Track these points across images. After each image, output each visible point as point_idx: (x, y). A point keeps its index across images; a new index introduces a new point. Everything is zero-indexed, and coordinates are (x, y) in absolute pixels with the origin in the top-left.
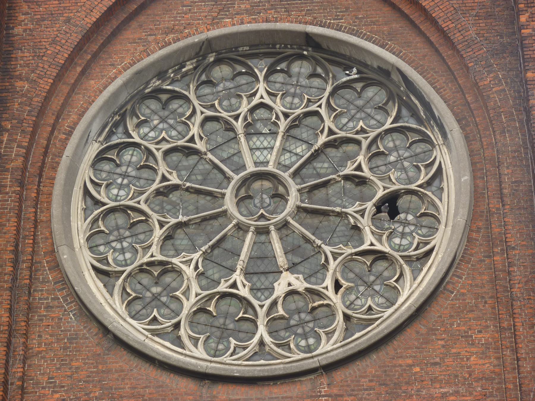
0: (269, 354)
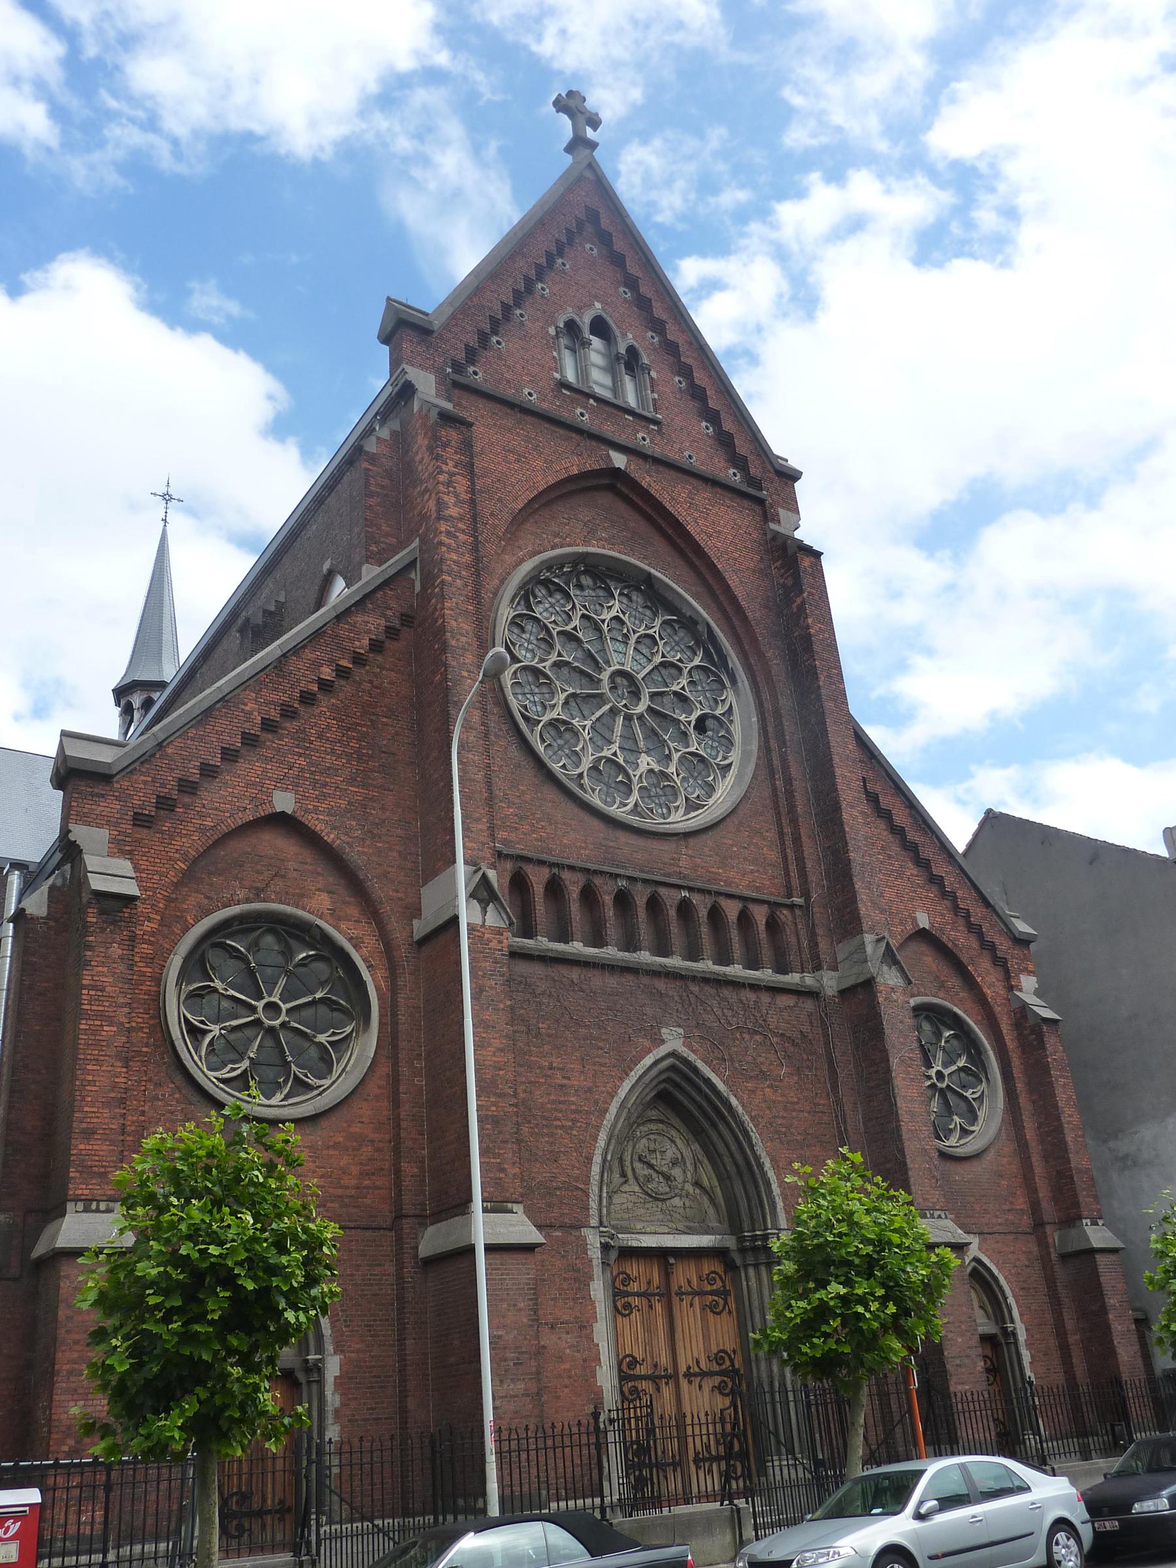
0: (639, 813)
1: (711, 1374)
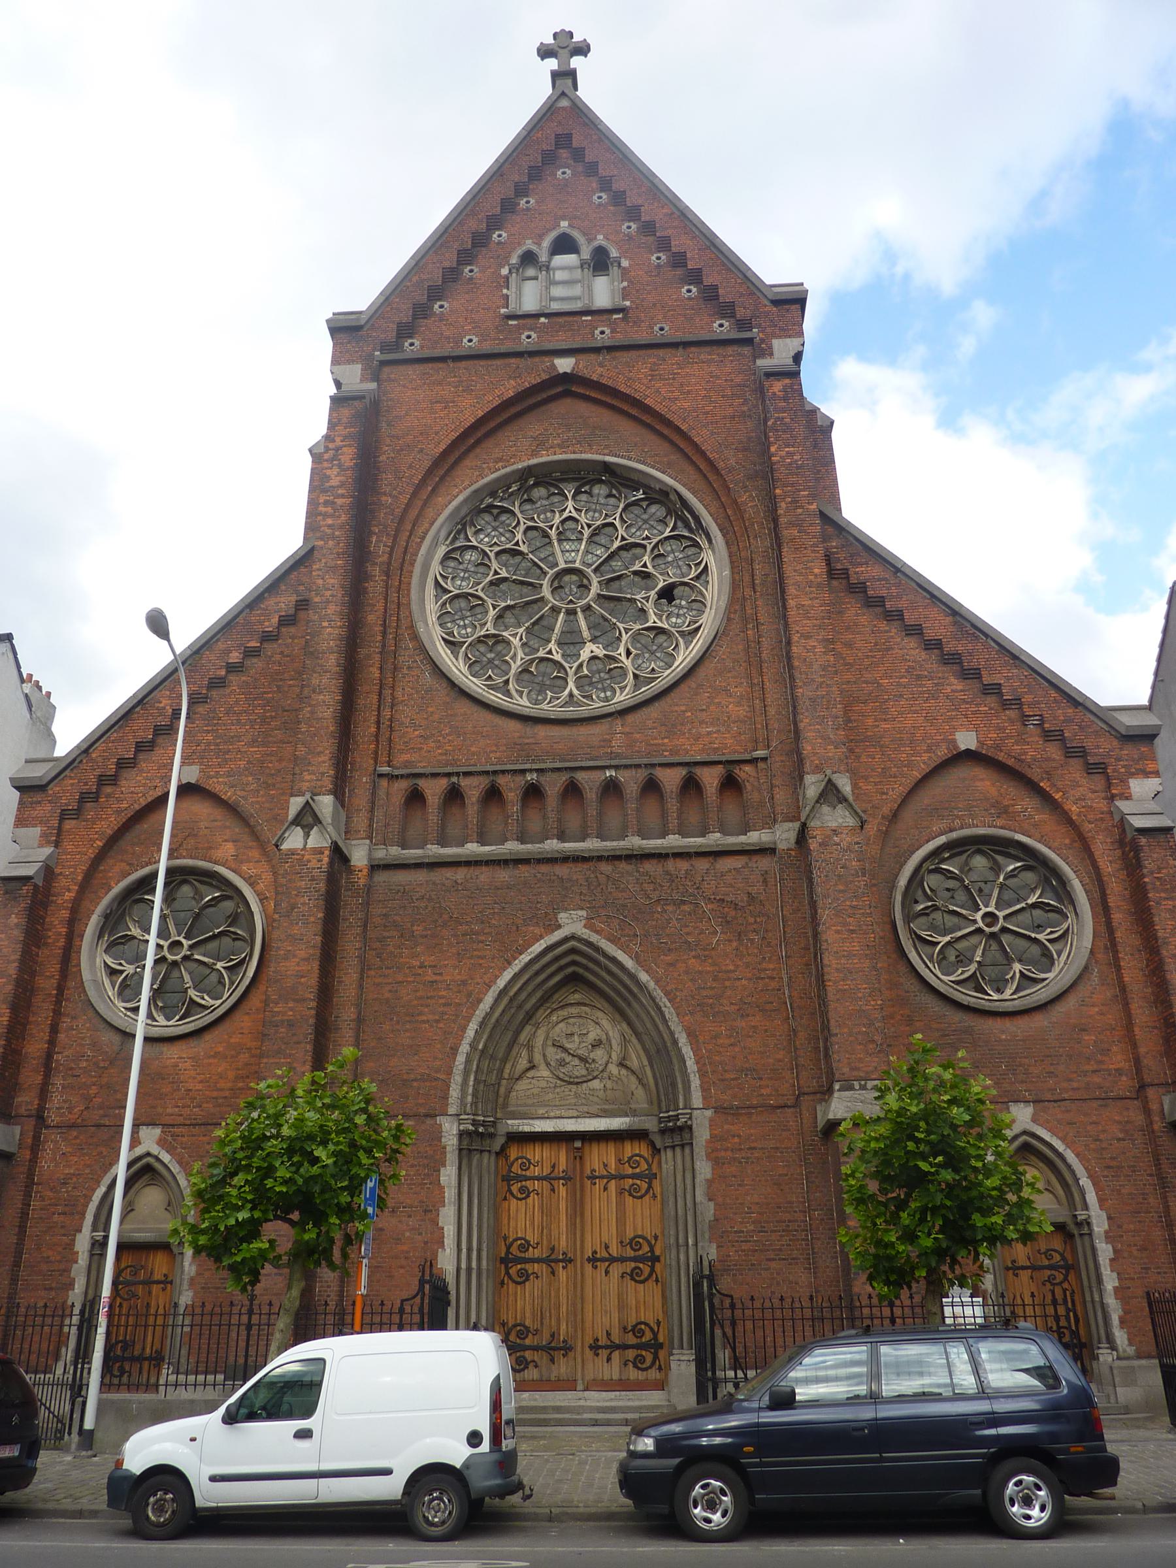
1: (622, 1260)
